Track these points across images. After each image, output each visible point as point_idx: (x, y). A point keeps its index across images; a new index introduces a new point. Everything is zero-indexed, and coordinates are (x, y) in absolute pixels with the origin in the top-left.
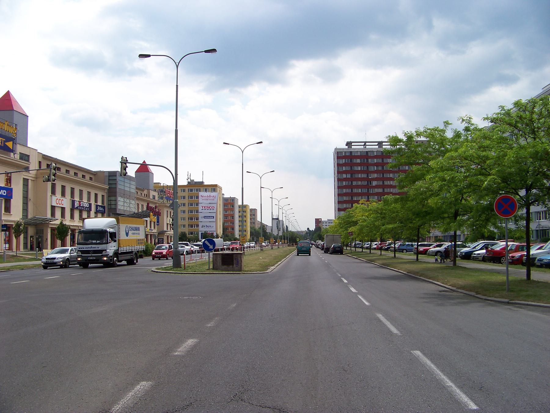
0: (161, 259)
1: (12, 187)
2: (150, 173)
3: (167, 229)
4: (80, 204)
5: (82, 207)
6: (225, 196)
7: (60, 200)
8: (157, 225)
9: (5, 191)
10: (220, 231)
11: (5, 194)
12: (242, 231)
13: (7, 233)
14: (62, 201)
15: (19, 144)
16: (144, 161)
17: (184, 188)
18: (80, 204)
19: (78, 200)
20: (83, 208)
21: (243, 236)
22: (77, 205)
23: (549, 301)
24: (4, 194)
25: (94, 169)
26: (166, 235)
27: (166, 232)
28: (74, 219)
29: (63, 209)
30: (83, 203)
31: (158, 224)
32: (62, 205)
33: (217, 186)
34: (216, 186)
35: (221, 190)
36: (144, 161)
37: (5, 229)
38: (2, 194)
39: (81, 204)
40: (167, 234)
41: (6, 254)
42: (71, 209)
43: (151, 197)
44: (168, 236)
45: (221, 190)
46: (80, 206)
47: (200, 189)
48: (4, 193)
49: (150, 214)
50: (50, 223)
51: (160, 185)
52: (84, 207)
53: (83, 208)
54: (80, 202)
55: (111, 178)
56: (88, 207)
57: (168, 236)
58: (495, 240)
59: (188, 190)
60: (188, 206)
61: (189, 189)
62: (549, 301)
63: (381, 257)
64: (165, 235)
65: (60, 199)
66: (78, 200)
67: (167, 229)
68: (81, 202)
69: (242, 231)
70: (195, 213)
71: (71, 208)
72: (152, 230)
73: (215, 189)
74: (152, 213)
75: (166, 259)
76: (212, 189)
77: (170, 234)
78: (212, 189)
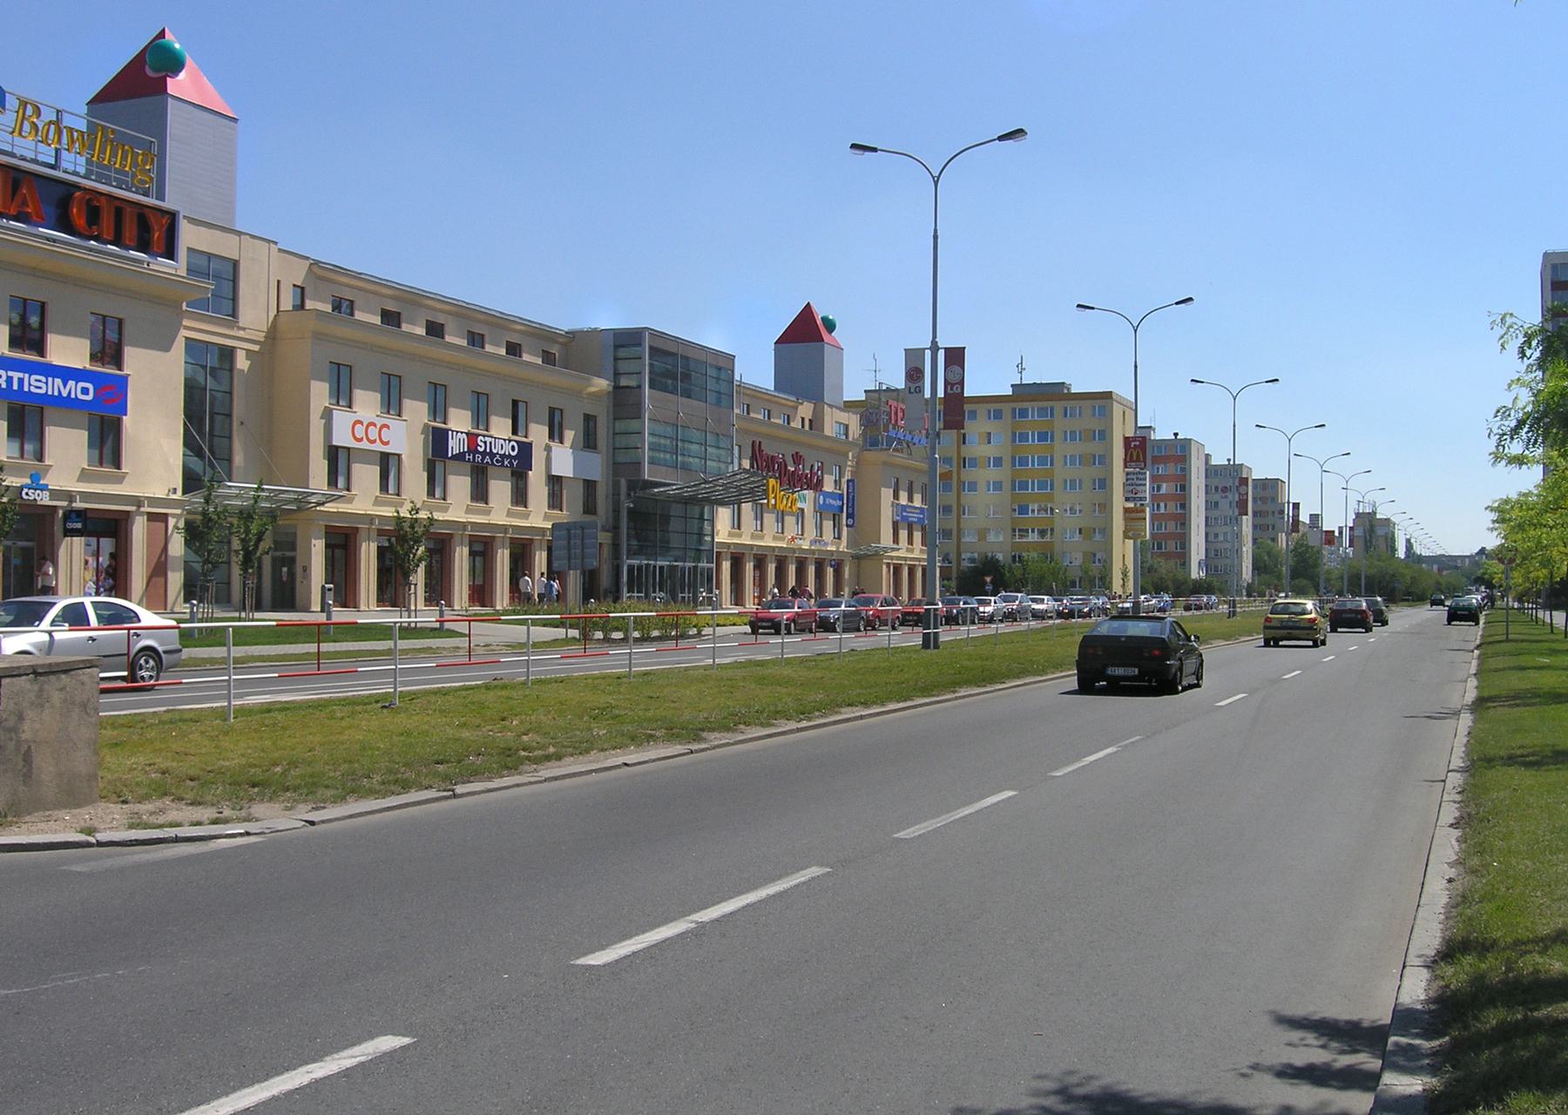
0: (1281, 643)
1: (126, 372)
5: (484, 454)
6: (1214, 462)
7: (371, 428)
8: (847, 526)
9: (90, 386)
10: (1124, 548)
11: (90, 397)
13: (107, 544)
14: (385, 429)
16: (809, 303)
17: (998, 406)
19: (467, 427)
21: (396, 568)
24: (81, 397)
25: (563, 321)
28: (487, 503)
30: (488, 440)
31: (850, 521)
32: (387, 443)
33: (1111, 398)
37: (79, 526)
38: (73, 396)
39: (480, 443)
40: (892, 558)
42: (429, 460)
46: (473, 447)
47: (1052, 409)
48: (85, 391)
49: (767, 485)
50: (318, 508)
51: (1066, 391)
52: (492, 455)
55: (622, 353)
56: (513, 454)
60: (1010, 465)
61: (1014, 410)
63: (1552, 637)
64: (885, 561)
65: (373, 424)
66: (467, 427)
68: (480, 438)
70: (1036, 490)
71: (430, 457)
72: (826, 544)
76: (989, 411)
77: (905, 559)
78: (989, 411)
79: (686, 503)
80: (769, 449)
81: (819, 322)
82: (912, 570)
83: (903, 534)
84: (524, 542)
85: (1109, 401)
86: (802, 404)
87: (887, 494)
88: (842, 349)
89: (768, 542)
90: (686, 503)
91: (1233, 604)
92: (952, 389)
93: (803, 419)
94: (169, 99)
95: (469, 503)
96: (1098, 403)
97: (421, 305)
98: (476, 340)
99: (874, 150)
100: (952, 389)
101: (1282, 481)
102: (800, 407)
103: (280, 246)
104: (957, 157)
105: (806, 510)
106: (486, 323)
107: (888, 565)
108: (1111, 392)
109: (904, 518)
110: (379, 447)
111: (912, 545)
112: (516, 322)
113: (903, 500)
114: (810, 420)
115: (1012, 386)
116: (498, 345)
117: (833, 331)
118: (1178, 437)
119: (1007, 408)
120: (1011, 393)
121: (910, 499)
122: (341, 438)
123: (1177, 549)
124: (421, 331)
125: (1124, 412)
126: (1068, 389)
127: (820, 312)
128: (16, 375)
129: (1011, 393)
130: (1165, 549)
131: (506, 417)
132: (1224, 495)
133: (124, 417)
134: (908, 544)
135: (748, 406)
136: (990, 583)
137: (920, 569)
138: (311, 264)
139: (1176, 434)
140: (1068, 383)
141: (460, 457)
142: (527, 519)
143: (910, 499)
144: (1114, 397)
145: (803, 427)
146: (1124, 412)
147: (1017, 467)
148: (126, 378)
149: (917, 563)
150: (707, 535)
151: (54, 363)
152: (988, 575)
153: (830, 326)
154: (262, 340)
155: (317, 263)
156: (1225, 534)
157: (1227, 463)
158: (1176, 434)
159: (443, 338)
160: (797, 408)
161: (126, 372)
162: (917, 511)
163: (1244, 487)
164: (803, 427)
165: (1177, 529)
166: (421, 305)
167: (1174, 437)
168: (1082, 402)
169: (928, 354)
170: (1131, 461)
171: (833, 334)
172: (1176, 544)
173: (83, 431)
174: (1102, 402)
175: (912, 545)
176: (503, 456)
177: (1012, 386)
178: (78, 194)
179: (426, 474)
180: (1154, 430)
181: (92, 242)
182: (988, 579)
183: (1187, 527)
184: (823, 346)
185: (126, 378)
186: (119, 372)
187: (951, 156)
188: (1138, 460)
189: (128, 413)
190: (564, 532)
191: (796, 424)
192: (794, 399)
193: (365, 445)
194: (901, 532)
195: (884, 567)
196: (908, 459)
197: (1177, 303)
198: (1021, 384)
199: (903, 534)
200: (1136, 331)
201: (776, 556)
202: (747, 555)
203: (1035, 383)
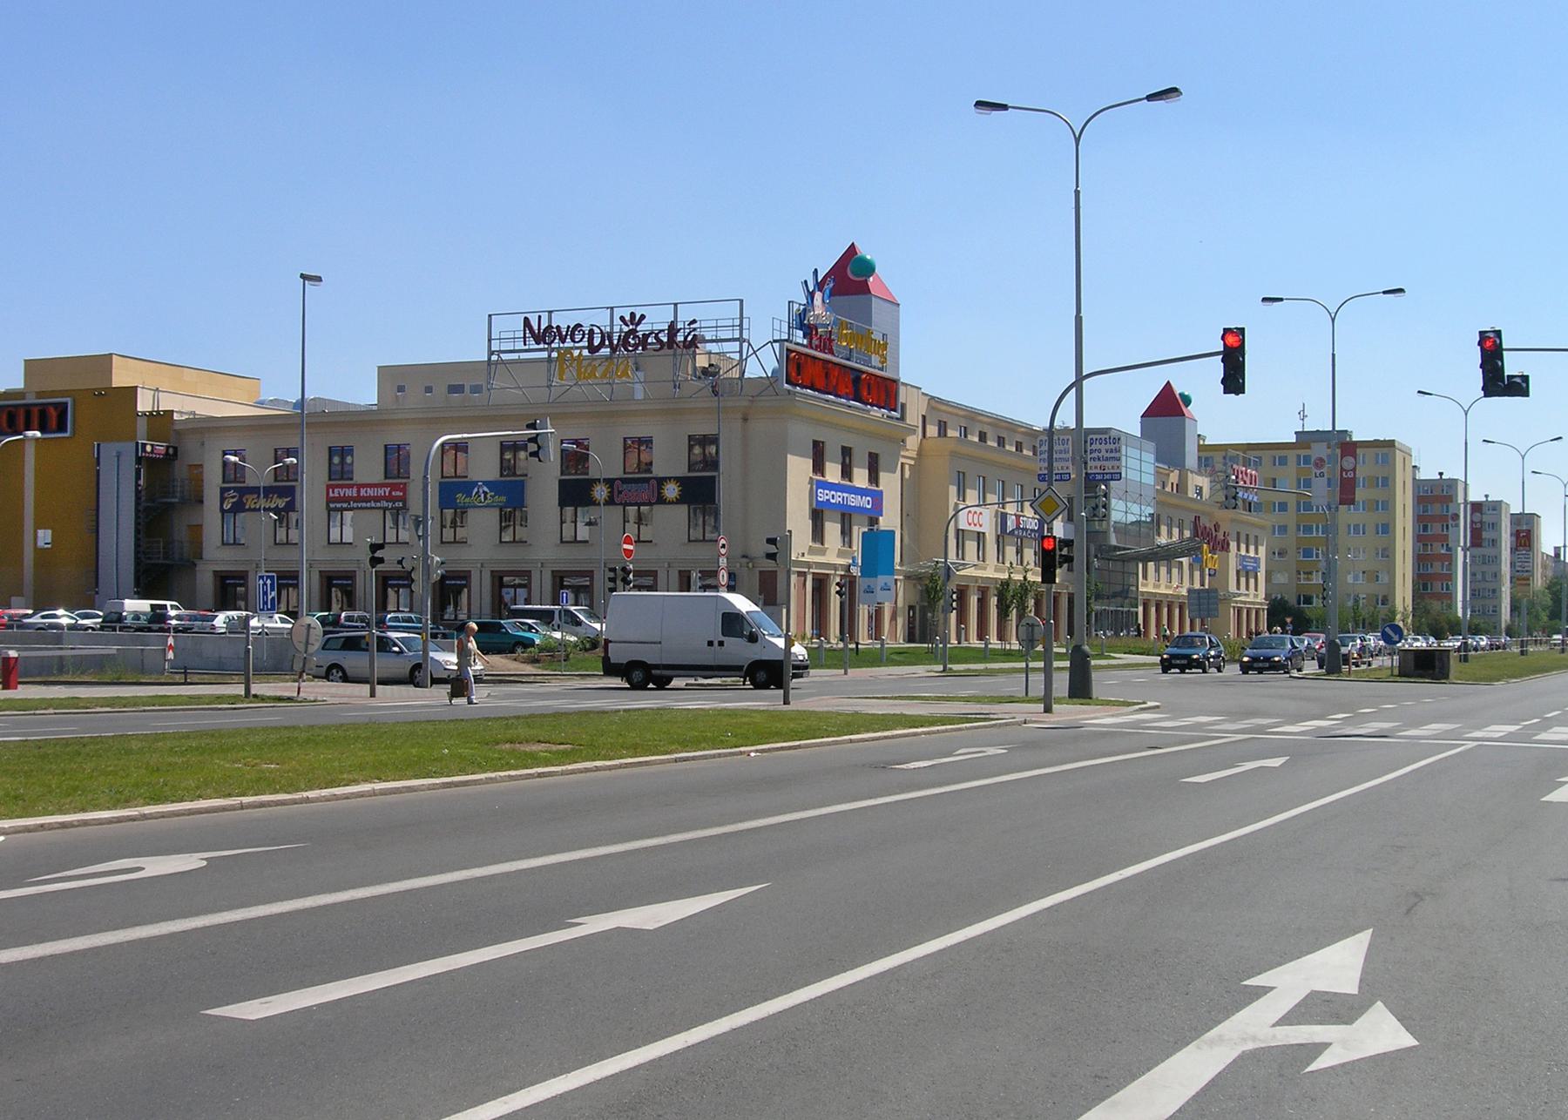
1: (881, 488)
2: (1187, 419)
3: (1238, 588)
4: (1018, 523)
5: (1023, 529)
6: (1422, 475)
11: (869, 507)
12: (1483, 593)
15: (1314, 442)
16: (1168, 382)
18: (1018, 523)
20: (1024, 534)
22: (1011, 525)
23: (87, 1119)
26: (1234, 607)
27: (959, 567)
28: (822, 544)
29: (980, 537)
30: (1025, 519)
33: (1394, 446)
34: (1390, 444)
35: (1407, 456)
36: (1168, 382)
40: (1236, 602)
41: (887, 648)
43: (1192, 494)
44: (1239, 611)
45: (1407, 457)
46: (1018, 527)
51: (1348, 439)
52: (1027, 530)
53: (1024, 534)
54: (1018, 517)
56: (1036, 528)
57: (1239, 611)
58: (1498, 342)
59: (1295, 459)
61: (1299, 456)
62: (87, 1119)
67: (1238, 588)
69: (1483, 593)
73: (1387, 455)
74: (1208, 543)
75: (1201, 671)
76: (1377, 455)
77: (1245, 603)
78: (1377, 455)
79: (1124, 561)
80: (1205, 521)
81: (1178, 396)
82: (1257, 611)
83: (1243, 580)
84: (821, 577)
85: (1393, 449)
86: (1172, 471)
87: (799, 469)
88: (1196, 421)
89: (1163, 591)
90: (1124, 561)
91: (1522, 644)
92: (1346, 474)
93: (1172, 484)
94: (873, 298)
95: (811, 544)
96: (1380, 451)
97: (1015, 431)
98: (1001, 441)
99: (1004, 107)
100: (1346, 474)
101: (1538, 516)
102: (1171, 474)
103: (923, 390)
104: (1104, 112)
105: (987, 534)
106: (1007, 429)
107: (802, 574)
108: (1394, 441)
109: (1244, 567)
110: (978, 529)
111: (1146, 580)
112: (982, 415)
113: (1243, 552)
114: (1177, 485)
115: (1296, 433)
116: (1011, 445)
117: (1189, 404)
118: (1444, 477)
119: (1291, 455)
120: (1294, 441)
121: (1247, 551)
122: (963, 525)
123: (1443, 589)
124: (976, 439)
125: (1404, 459)
126: (1350, 436)
127: (1178, 389)
128: (845, 495)
129: (1294, 441)
130: (1431, 589)
131: (864, 468)
132: (1318, 472)
133: (881, 518)
134: (814, 540)
135: (965, 428)
136: (1291, 623)
137: (1245, 611)
138: (929, 400)
139: (1441, 474)
140: (1349, 430)
141: (1012, 532)
142: (824, 554)
143: (1247, 551)
144: (1396, 444)
145: (1172, 490)
146: (1404, 459)
147: (1302, 512)
148: (881, 492)
149: (1252, 606)
150: (1133, 585)
151: (830, 481)
152: (1289, 616)
153: (1187, 401)
154: (915, 456)
155: (933, 398)
156: (1483, 573)
157: (1484, 499)
158: (1441, 474)
159: (986, 442)
160: (1169, 475)
161: (881, 488)
162: (1252, 560)
163: (1351, 459)
164: (1172, 490)
165: (1442, 570)
166: (1015, 431)
167: (1439, 477)
168: (1366, 449)
169: (1562, 549)
170: (1521, 545)
171: (1189, 408)
172: (1442, 584)
173: (836, 525)
174: (1385, 450)
175: (1146, 580)
176: (1032, 530)
177: (1296, 433)
178: (864, 376)
179: (811, 522)
180: (1419, 469)
181: (809, 391)
182: (1289, 620)
183: (1453, 567)
184: (1184, 421)
185: (881, 492)
186: (876, 488)
187: (1098, 110)
188: (1525, 545)
189: (884, 513)
190: (1196, 595)
191: (1168, 489)
192: (1166, 467)
193: (972, 528)
194: (968, 543)
195: (1232, 610)
196: (1247, 515)
197: (1384, 292)
198: (1303, 432)
199: (1243, 580)
200: (1466, 414)
201: (979, 587)
202: (972, 588)
203: (1318, 431)
